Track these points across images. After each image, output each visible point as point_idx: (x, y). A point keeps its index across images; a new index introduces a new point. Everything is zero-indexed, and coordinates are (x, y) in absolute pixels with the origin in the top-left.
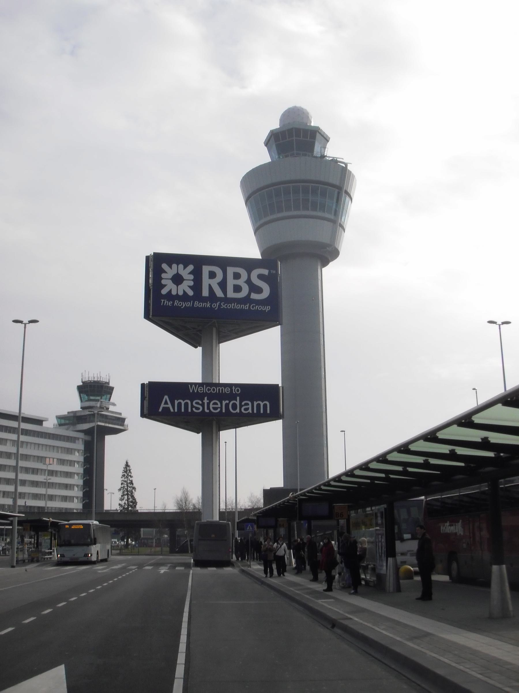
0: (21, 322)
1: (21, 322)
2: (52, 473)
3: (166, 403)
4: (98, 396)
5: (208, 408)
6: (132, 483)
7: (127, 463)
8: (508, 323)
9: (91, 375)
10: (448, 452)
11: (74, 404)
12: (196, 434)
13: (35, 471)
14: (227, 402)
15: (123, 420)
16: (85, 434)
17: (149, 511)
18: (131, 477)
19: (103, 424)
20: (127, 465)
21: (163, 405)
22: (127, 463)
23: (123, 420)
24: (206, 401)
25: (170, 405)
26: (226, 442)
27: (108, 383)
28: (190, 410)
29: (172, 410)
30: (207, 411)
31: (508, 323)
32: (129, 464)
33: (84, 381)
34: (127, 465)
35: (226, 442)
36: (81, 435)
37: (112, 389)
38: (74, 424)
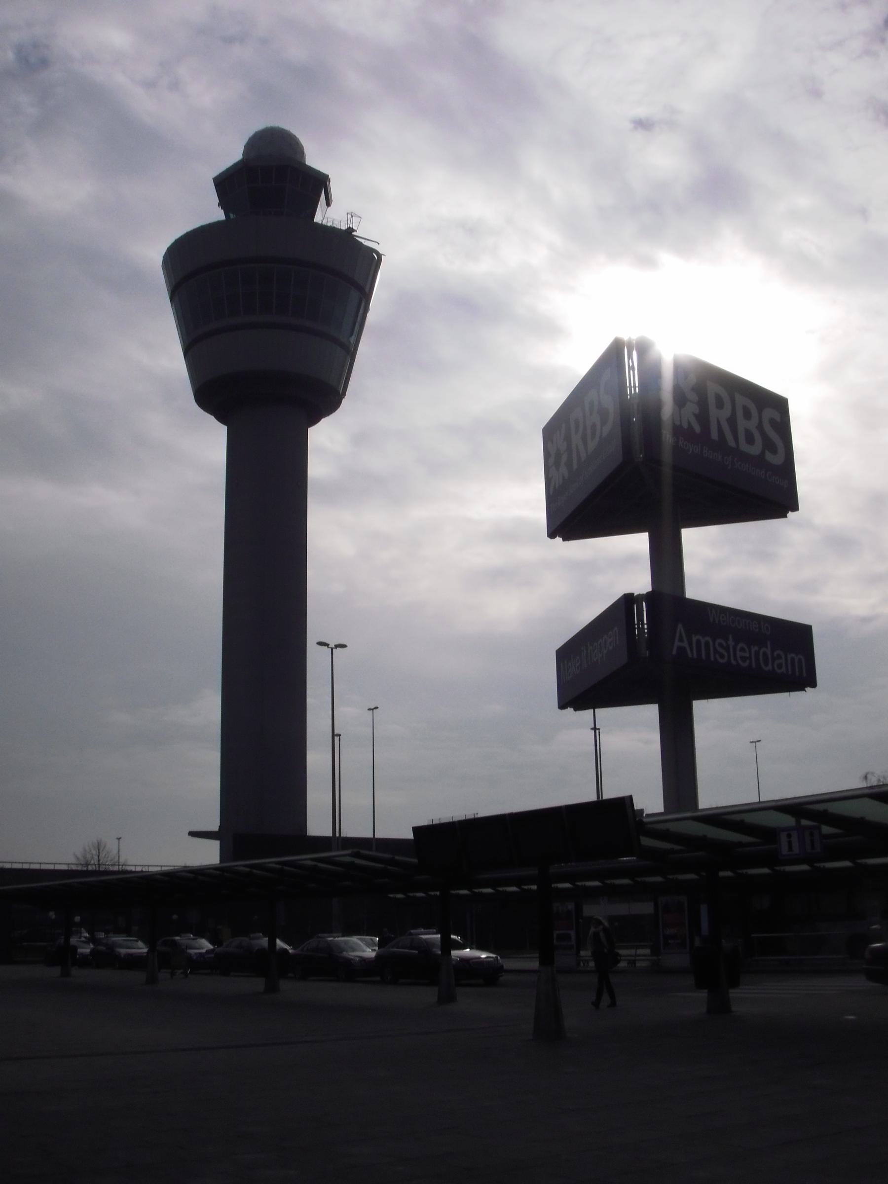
0: (326, 645)
1: (326, 645)
3: (681, 640)
5: (735, 659)
8: (343, 646)
10: (410, 836)
12: (216, 200)
14: (756, 648)
21: (677, 643)
24: (731, 643)
25: (685, 644)
26: (119, 839)
28: (712, 659)
29: (690, 656)
30: (734, 662)
31: (343, 646)
35: (119, 839)
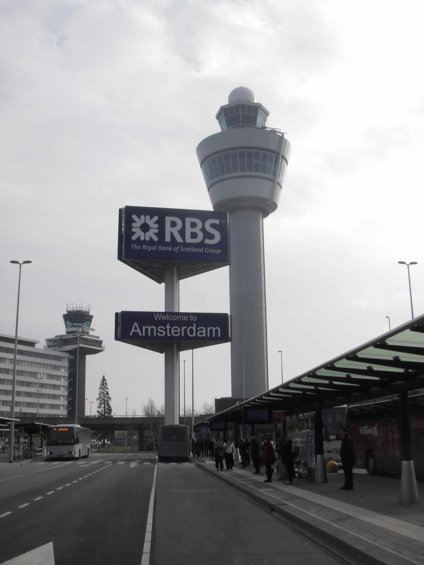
0: (17, 262)
1: (17, 262)
2: (42, 386)
3: (136, 328)
4: (80, 323)
5: (170, 333)
6: (107, 394)
7: (104, 377)
8: (415, 263)
9: (74, 306)
10: (366, 369)
11: (60, 329)
12: (160, 354)
13: (28, 384)
14: (186, 327)
15: (100, 343)
16: (69, 354)
17: (122, 417)
18: (107, 389)
19: (84, 346)
20: (104, 379)
21: (133, 330)
22: (104, 377)
23: (100, 343)
24: (168, 327)
25: (139, 331)
26: (184, 361)
27: (89, 312)
28: (155, 335)
29: (140, 334)
30: (169, 335)
31: (415, 263)
32: (105, 378)
33: (68, 310)
34: (104, 379)
35: (184, 361)
36: (66, 355)
37: (92, 317)
38: (60, 346)
